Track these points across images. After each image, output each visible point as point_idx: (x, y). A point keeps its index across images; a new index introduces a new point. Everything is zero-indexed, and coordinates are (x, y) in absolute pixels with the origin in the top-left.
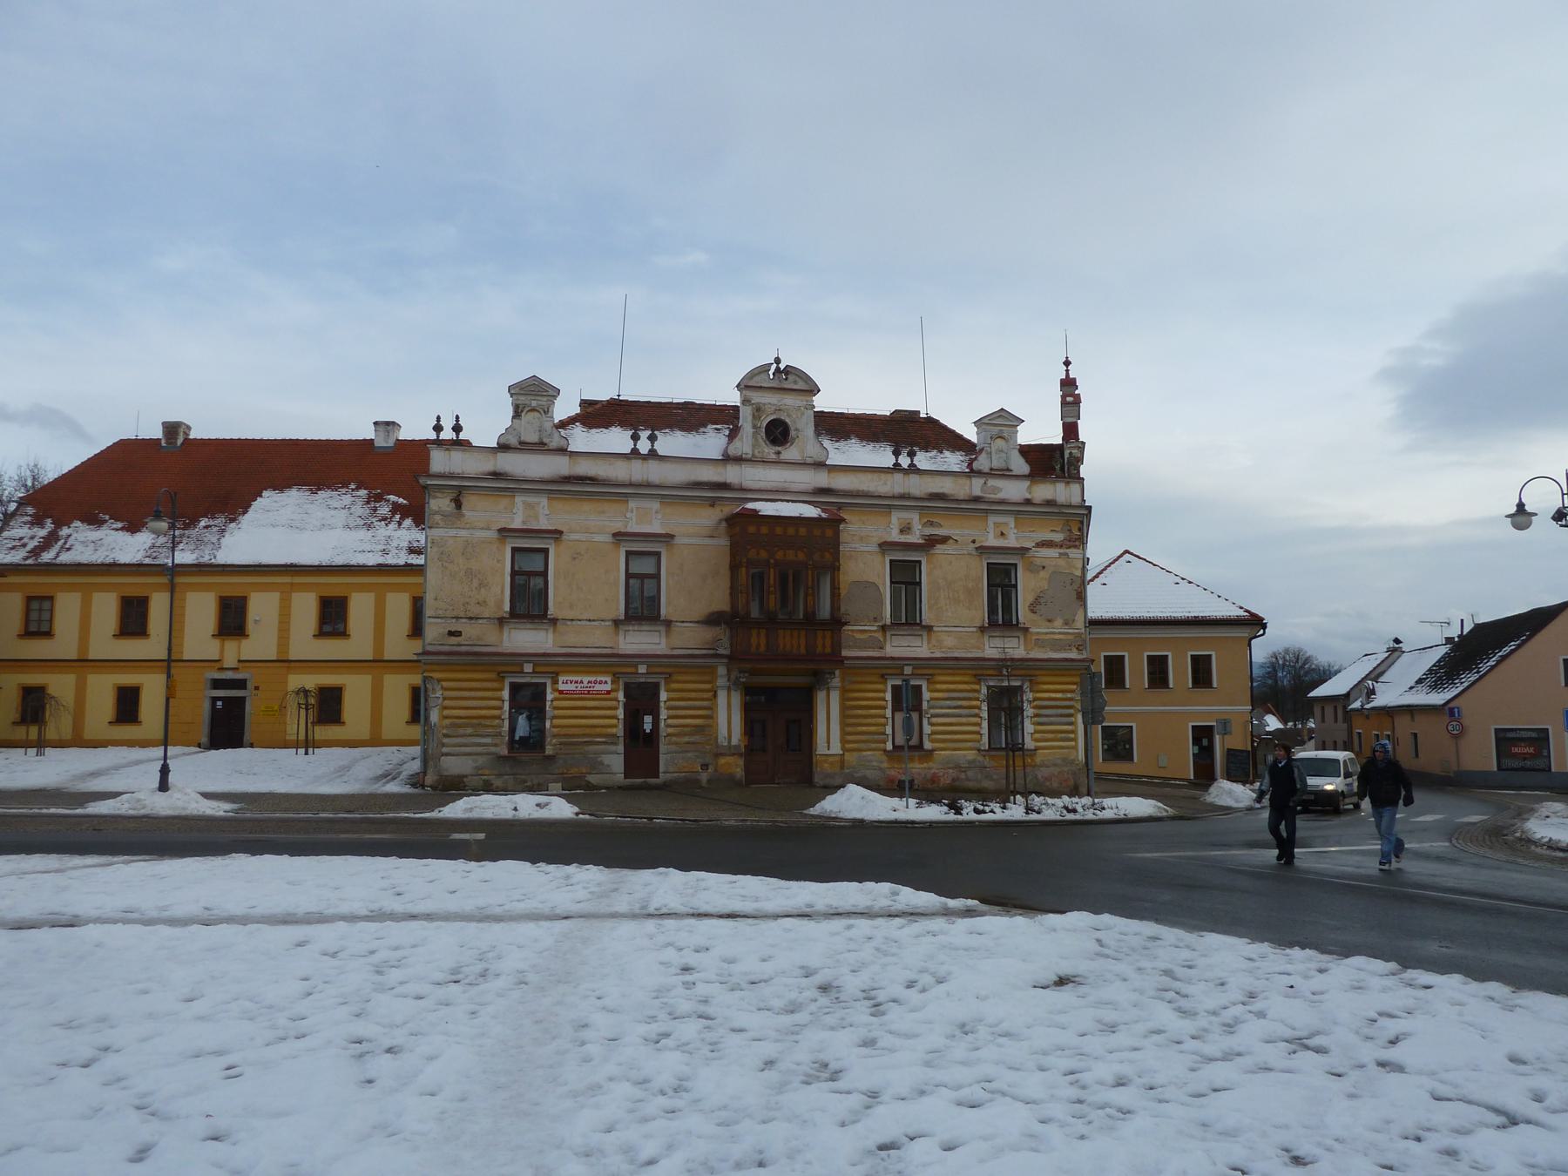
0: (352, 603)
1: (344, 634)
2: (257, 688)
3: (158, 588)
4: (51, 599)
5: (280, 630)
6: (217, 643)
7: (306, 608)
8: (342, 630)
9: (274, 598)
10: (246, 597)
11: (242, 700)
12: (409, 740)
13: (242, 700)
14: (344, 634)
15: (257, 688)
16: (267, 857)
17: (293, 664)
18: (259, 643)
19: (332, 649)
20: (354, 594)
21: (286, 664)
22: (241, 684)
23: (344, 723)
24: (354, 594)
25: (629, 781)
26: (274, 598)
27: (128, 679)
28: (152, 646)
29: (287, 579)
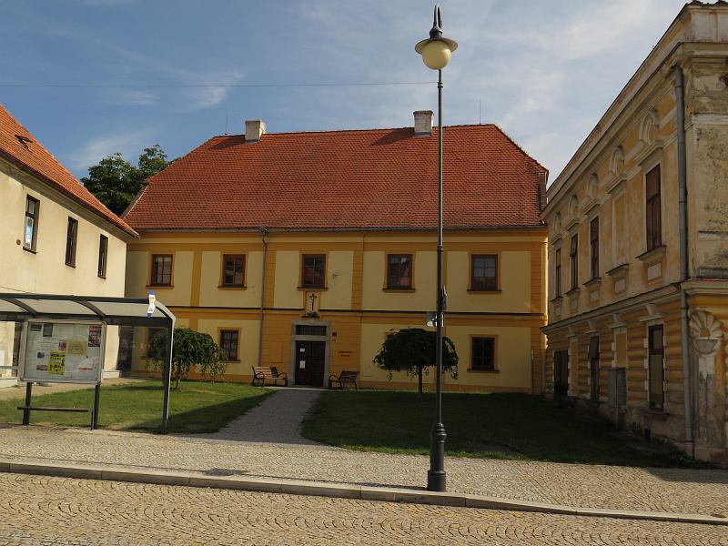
0: (329, 260)
1: (409, 288)
2: (335, 334)
3: (255, 247)
4: (495, 257)
5: (361, 291)
6: (301, 294)
7: (376, 264)
8: (407, 284)
9: (190, 255)
10: (411, 255)
11: (323, 344)
12: (14, 351)
13: (323, 344)
14: (409, 288)
15: (335, 334)
16: (627, 473)
17: (365, 314)
18: (336, 295)
19: (483, 303)
20: (250, 253)
21: (360, 314)
22: (322, 330)
23: (498, 371)
24: (250, 253)
25: (126, 381)
26: (190, 255)
27: (229, 324)
28: (247, 297)
29: (359, 239)
